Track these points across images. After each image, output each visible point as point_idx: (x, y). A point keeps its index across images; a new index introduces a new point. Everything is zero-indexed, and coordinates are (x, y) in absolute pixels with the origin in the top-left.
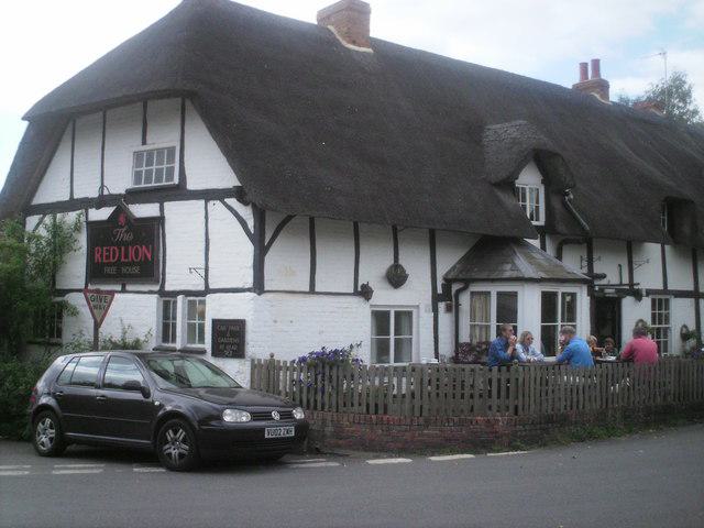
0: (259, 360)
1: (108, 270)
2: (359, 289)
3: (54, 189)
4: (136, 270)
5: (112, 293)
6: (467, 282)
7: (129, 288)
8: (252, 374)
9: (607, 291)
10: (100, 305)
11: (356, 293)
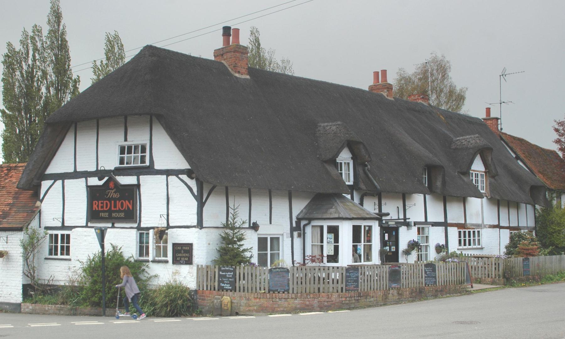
0: (202, 266)
1: (102, 215)
2: (251, 225)
4: (122, 215)
5: (106, 228)
6: (310, 220)
8: (197, 273)
9: (390, 223)
11: (250, 228)
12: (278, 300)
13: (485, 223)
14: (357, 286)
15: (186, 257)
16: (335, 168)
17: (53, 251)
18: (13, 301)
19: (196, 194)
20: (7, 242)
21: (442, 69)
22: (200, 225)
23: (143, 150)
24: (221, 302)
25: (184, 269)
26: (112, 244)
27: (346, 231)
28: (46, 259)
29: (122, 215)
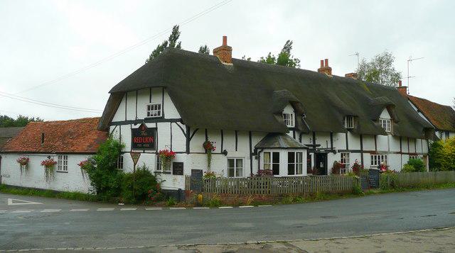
3: (119, 117)
6: (263, 149)
10: (135, 157)
11: (222, 153)
21: (385, 61)
23: (159, 108)
25: (179, 177)
27: (284, 157)
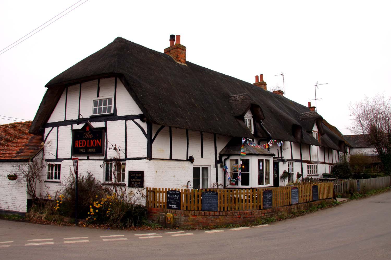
1: (81, 150)
2: (189, 158)
4: (94, 150)
6: (229, 156)
7: (90, 158)
11: (187, 160)
12: (211, 217)
13: (319, 161)
14: (271, 204)
15: (139, 182)
16: (243, 122)
17: (50, 176)
18: (21, 211)
19: (147, 133)
20: (19, 170)
22: (149, 157)
23: (110, 103)
24: (165, 217)
26: (87, 172)
28: (46, 181)
29: (94, 150)
